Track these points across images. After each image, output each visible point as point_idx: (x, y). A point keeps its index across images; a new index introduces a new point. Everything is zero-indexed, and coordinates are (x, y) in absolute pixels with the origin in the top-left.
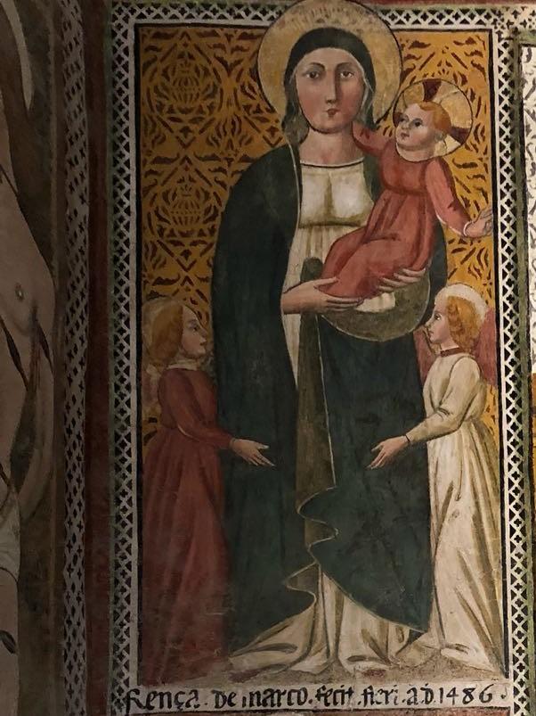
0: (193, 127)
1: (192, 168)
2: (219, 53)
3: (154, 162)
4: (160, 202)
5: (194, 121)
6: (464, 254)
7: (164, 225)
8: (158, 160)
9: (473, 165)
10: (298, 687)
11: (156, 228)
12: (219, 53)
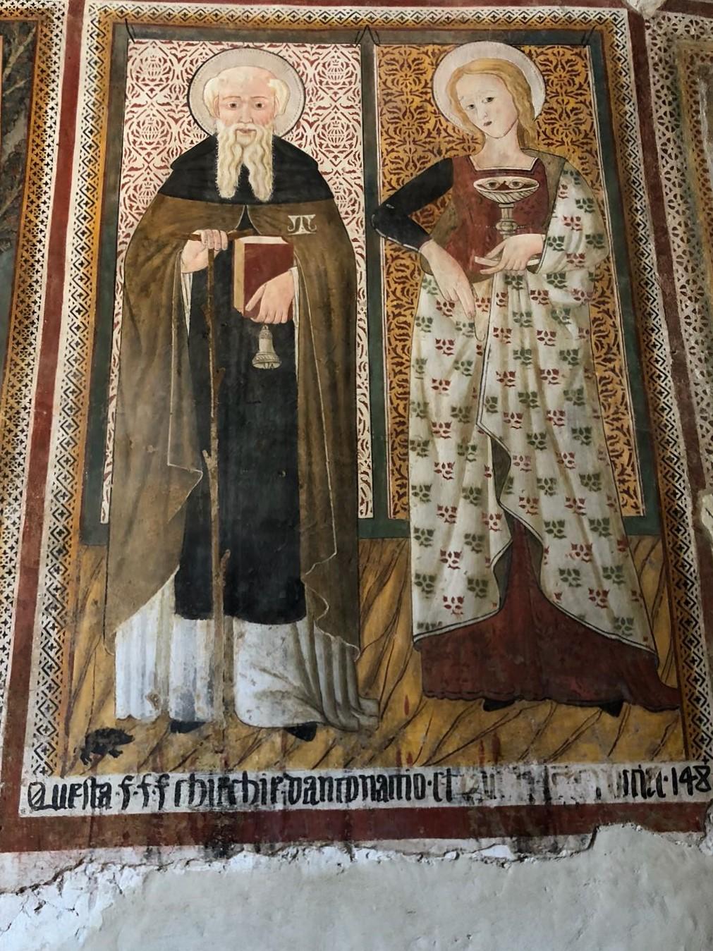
0: (153, 152)
1: (152, 174)
2: (172, 114)
3: (130, 170)
4: (134, 127)
5: (155, 149)
6: (344, 90)
7: (133, 204)
8: (132, 169)
9: (354, 172)
10: (310, 806)
11: (128, 205)
12: (174, 51)
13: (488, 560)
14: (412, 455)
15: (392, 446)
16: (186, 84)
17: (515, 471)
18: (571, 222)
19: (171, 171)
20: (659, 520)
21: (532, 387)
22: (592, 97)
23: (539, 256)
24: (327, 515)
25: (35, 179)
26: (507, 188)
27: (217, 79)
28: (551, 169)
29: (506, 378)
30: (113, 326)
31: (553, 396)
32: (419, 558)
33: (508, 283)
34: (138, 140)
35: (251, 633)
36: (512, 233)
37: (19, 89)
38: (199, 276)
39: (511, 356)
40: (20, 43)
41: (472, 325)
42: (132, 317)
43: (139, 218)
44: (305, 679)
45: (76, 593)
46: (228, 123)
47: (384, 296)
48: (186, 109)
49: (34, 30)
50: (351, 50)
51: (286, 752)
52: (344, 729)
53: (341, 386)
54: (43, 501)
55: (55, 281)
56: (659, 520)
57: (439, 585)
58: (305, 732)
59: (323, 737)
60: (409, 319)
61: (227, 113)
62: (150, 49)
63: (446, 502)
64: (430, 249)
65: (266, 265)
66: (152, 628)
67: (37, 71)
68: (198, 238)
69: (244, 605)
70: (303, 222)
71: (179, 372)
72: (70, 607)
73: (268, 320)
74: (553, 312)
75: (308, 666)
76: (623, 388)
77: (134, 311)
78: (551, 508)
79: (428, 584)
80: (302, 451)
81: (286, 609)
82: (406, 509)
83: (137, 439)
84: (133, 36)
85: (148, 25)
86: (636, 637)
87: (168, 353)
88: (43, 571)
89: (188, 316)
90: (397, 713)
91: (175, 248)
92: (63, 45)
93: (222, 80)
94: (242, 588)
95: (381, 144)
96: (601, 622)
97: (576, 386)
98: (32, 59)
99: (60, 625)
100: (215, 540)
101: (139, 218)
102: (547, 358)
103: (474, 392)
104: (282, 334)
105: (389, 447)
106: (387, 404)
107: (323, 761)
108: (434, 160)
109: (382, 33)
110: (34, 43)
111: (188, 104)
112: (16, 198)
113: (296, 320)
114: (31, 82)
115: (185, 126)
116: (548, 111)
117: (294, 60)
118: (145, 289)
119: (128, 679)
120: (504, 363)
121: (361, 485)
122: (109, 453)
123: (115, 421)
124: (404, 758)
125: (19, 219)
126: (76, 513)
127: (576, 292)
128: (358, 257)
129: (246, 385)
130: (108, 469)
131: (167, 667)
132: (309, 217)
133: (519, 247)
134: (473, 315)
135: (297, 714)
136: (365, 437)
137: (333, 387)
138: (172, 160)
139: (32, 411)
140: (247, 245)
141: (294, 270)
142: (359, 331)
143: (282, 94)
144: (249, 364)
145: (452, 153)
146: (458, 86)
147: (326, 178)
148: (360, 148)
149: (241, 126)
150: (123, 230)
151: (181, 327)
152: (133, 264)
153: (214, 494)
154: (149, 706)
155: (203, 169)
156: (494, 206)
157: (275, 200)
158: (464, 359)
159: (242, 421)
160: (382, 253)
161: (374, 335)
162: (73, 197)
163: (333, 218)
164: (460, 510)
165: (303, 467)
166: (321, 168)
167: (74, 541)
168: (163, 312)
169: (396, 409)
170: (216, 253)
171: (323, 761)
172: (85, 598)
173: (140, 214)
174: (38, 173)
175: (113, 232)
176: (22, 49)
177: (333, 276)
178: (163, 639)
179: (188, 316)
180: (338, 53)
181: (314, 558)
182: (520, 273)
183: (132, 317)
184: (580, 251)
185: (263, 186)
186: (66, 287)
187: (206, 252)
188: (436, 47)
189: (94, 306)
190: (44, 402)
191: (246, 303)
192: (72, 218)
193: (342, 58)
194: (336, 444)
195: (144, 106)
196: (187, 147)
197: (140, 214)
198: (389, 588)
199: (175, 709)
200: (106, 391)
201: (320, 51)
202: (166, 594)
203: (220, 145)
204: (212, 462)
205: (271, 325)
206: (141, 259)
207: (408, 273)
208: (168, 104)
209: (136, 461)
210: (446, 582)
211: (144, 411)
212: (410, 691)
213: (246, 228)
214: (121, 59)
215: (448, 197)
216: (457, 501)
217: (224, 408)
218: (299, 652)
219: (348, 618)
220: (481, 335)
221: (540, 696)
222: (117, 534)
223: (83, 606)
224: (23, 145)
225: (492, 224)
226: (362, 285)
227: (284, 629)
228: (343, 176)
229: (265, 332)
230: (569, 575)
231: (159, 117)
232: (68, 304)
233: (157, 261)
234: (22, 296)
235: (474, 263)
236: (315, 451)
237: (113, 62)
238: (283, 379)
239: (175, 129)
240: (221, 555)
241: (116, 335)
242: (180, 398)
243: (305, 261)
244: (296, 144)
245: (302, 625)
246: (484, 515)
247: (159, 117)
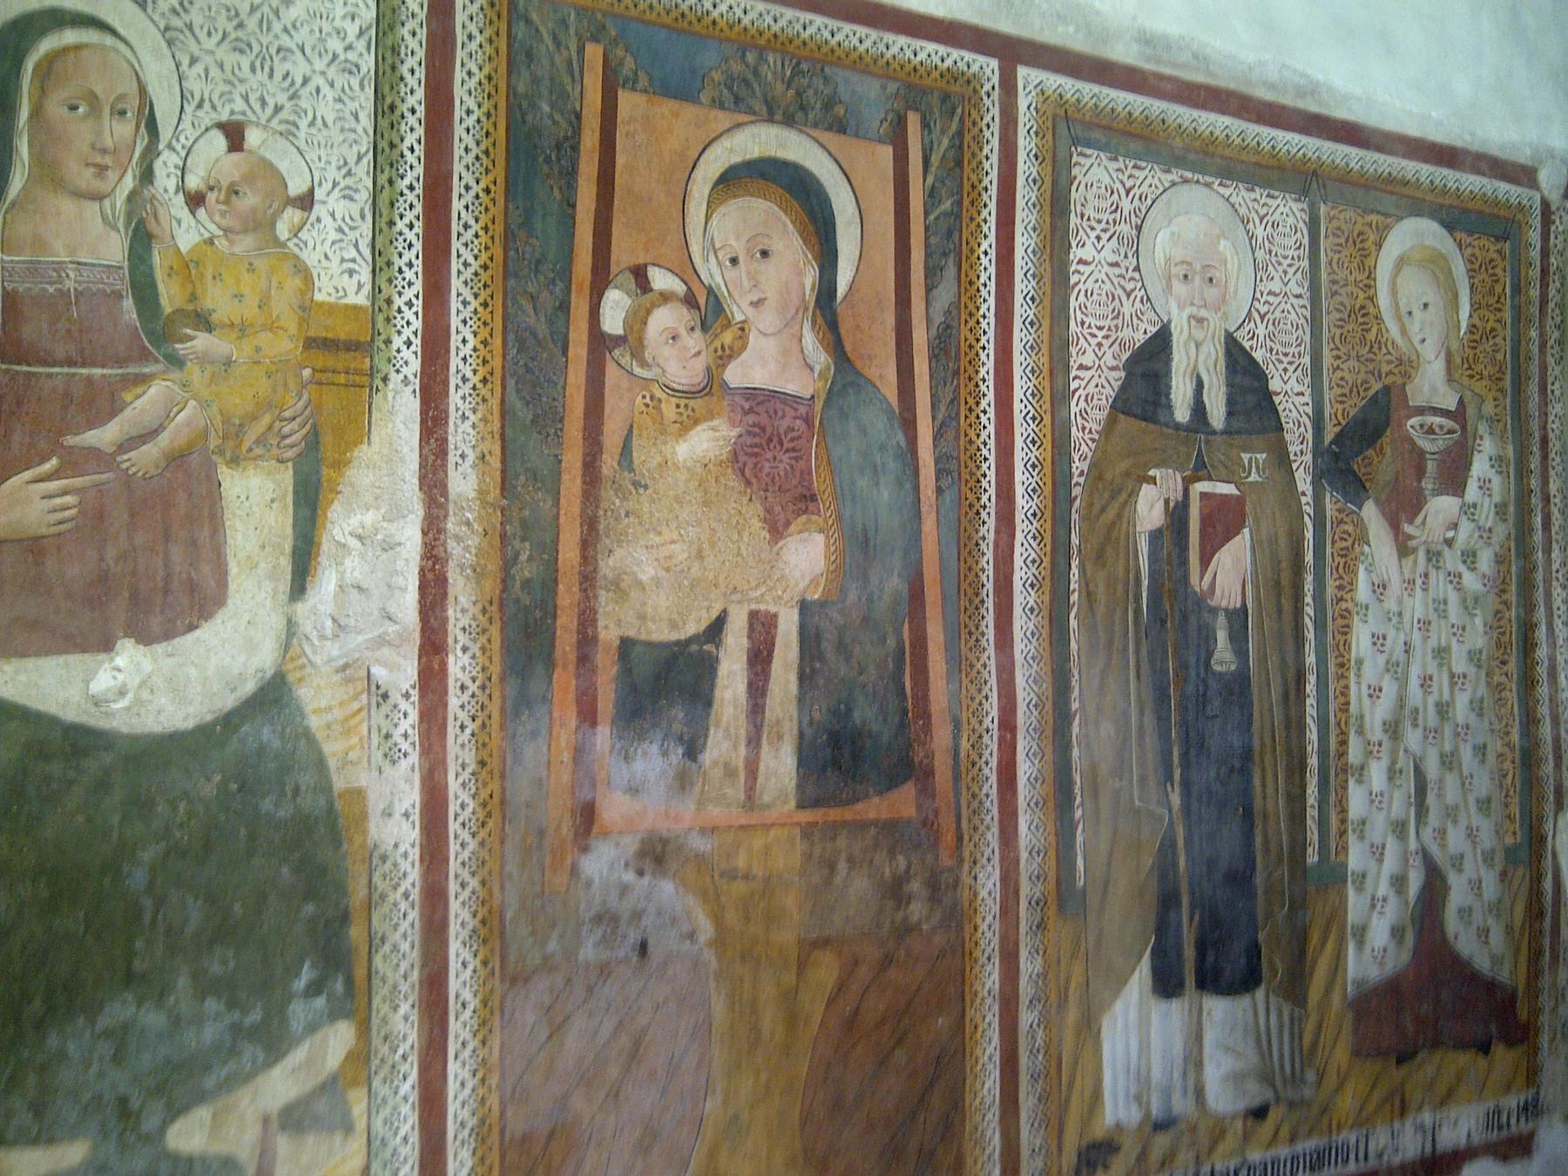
4: (1082, 298)
13: (1407, 903)
14: (1351, 783)
15: (1337, 772)
16: (1134, 232)
17: (1431, 799)
18: (1484, 485)
19: (1123, 374)
20: (1529, 851)
21: (1446, 696)
22: (1507, 315)
23: (1455, 526)
24: (1280, 860)
25: (971, 370)
26: (1433, 433)
27: (1168, 231)
28: (1471, 411)
29: (1426, 681)
30: (1069, 607)
31: (1462, 702)
32: (1355, 904)
33: (1429, 560)
34: (1087, 320)
35: (1217, 1008)
36: (1438, 492)
37: (945, 214)
38: (1155, 536)
39: (1430, 655)
40: (943, 132)
41: (1400, 614)
42: (1089, 595)
43: (1093, 446)
44: (1262, 1054)
45: (1058, 977)
46: (1181, 307)
47: (1328, 573)
48: (1136, 275)
49: (959, 110)
50: (1300, 205)
51: (1246, 1137)
52: (1291, 1105)
53: (1292, 693)
54: (1018, 861)
55: (1004, 537)
56: (1529, 851)
57: (1370, 935)
58: (1260, 1113)
59: (1273, 1116)
60: (1350, 605)
61: (1179, 287)
62: (1094, 169)
63: (1378, 840)
64: (1370, 512)
65: (1223, 521)
66: (1133, 1016)
67: (967, 187)
68: (1153, 480)
69: (1210, 982)
70: (1255, 461)
71: (1138, 676)
72: (1053, 999)
73: (1224, 604)
74: (1465, 601)
75: (1264, 1037)
76: (1512, 696)
77: (1091, 587)
78: (1456, 840)
79: (1361, 933)
80: (1257, 781)
81: (1247, 982)
82: (1345, 849)
83: (1104, 769)
84: (1076, 142)
85: (1090, 125)
86: (1504, 976)
87: (1125, 649)
88: (1024, 954)
89: (1145, 595)
90: (1332, 1078)
91: (1422, 928)
92: (995, 142)
93: (1173, 233)
94: (1210, 958)
95: (1327, 359)
96: (1482, 963)
97: (1479, 694)
98: (959, 163)
99: (1045, 1022)
100: (1185, 901)
101: (1093, 446)
102: (1460, 664)
103: (1401, 702)
104: (1238, 618)
105: (1332, 772)
106: (1332, 719)
107: (1274, 1140)
108: (1376, 386)
109: (1328, 183)
110: (960, 133)
111: (1137, 269)
112: (952, 401)
113: (1249, 606)
114: (960, 203)
115: (1138, 304)
116: (1472, 328)
117: (1243, 211)
118: (1100, 557)
119: (1115, 1078)
120: (1424, 665)
121: (1309, 822)
122: (1077, 790)
123: (1079, 745)
124: (1334, 1126)
125: (957, 438)
126: (1052, 874)
127: (1484, 576)
128: (1306, 518)
129: (1205, 694)
130: (1078, 814)
131: (1149, 1060)
132: (1262, 457)
133: (1441, 507)
134: (1400, 602)
135: (1256, 1093)
136: (1313, 761)
137: (1286, 696)
138: (1125, 357)
139: (996, 734)
140: (1204, 496)
141: (1246, 531)
142: (1307, 620)
143: (1232, 266)
144: (1208, 665)
145: (1391, 379)
146: (1399, 281)
147: (1276, 399)
148: (1307, 360)
149: (1194, 310)
150: (1079, 466)
151: (1138, 611)
152: (1088, 518)
153: (1181, 843)
154: (1134, 1108)
155: (1156, 376)
156: (1422, 453)
157: (1227, 432)
158: (1394, 659)
159: (1201, 745)
160: (1328, 514)
161: (1320, 625)
162: (1017, 406)
163: (1282, 459)
164: (1388, 846)
165: (1258, 804)
166: (1275, 385)
167: (1052, 910)
168: (1120, 587)
169: (1339, 724)
170: (1172, 504)
171: (1274, 1140)
172: (1068, 981)
173: (1093, 440)
174: (974, 362)
175: (1066, 467)
176: (946, 142)
177: (1283, 542)
178: (1144, 1023)
179: (1145, 595)
180: (1287, 210)
181: (1269, 915)
182: (1439, 547)
183: (1089, 594)
184: (1489, 525)
185: (1217, 414)
186: (1018, 550)
187: (1162, 502)
188: (1380, 218)
189: (1048, 579)
190: (1008, 724)
191: (1202, 578)
192: (1019, 442)
193: (1288, 211)
194: (1290, 773)
195: (1091, 254)
196: (1140, 338)
197: (1093, 440)
198: (1330, 946)
199: (1156, 1110)
200: (1067, 704)
201: (1269, 201)
202: (1142, 974)
203: (1174, 338)
204: (1176, 799)
205: (1226, 610)
206: (1097, 507)
207: (1349, 543)
208: (1116, 265)
209: (1105, 802)
210: (1372, 944)
211: (1107, 729)
212: (1341, 1054)
213: (1201, 470)
214: (1063, 181)
215: (1386, 440)
216: (1385, 838)
217: (1184, 724)
218: (1258, 1032)
219: (1295, 988)
220: (1407, 626)
221: (1436, 1044)
222: (1093, 900)
223: (1066, 995)
224: (955, 312)
225: (1419, 481)
226: (1309, 558)
227: (1244, 1001)
228: (1291, 394)
229: (1222, 619)
230: (1465, 913)
231: (1108, 287)
232: (1020, 575)
233: (1111, 514)
234: (970, 560)
235: (1404, 533)
236: (1269, 779)
237: (1054, 183)
238: (1238, 687)
239: (1127, 309)
240: (1191, 919)
241: (1073, 623)
242: (1142, 712)
243: (1257, 520)
244: (1247, 345)
245: (1260, 994)
246: (1406, 852)
247: (1108, 287)
